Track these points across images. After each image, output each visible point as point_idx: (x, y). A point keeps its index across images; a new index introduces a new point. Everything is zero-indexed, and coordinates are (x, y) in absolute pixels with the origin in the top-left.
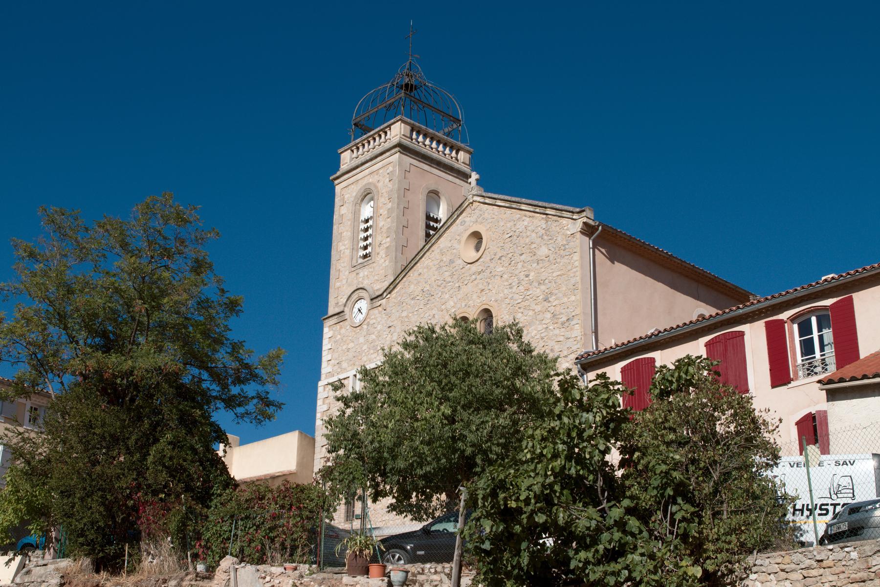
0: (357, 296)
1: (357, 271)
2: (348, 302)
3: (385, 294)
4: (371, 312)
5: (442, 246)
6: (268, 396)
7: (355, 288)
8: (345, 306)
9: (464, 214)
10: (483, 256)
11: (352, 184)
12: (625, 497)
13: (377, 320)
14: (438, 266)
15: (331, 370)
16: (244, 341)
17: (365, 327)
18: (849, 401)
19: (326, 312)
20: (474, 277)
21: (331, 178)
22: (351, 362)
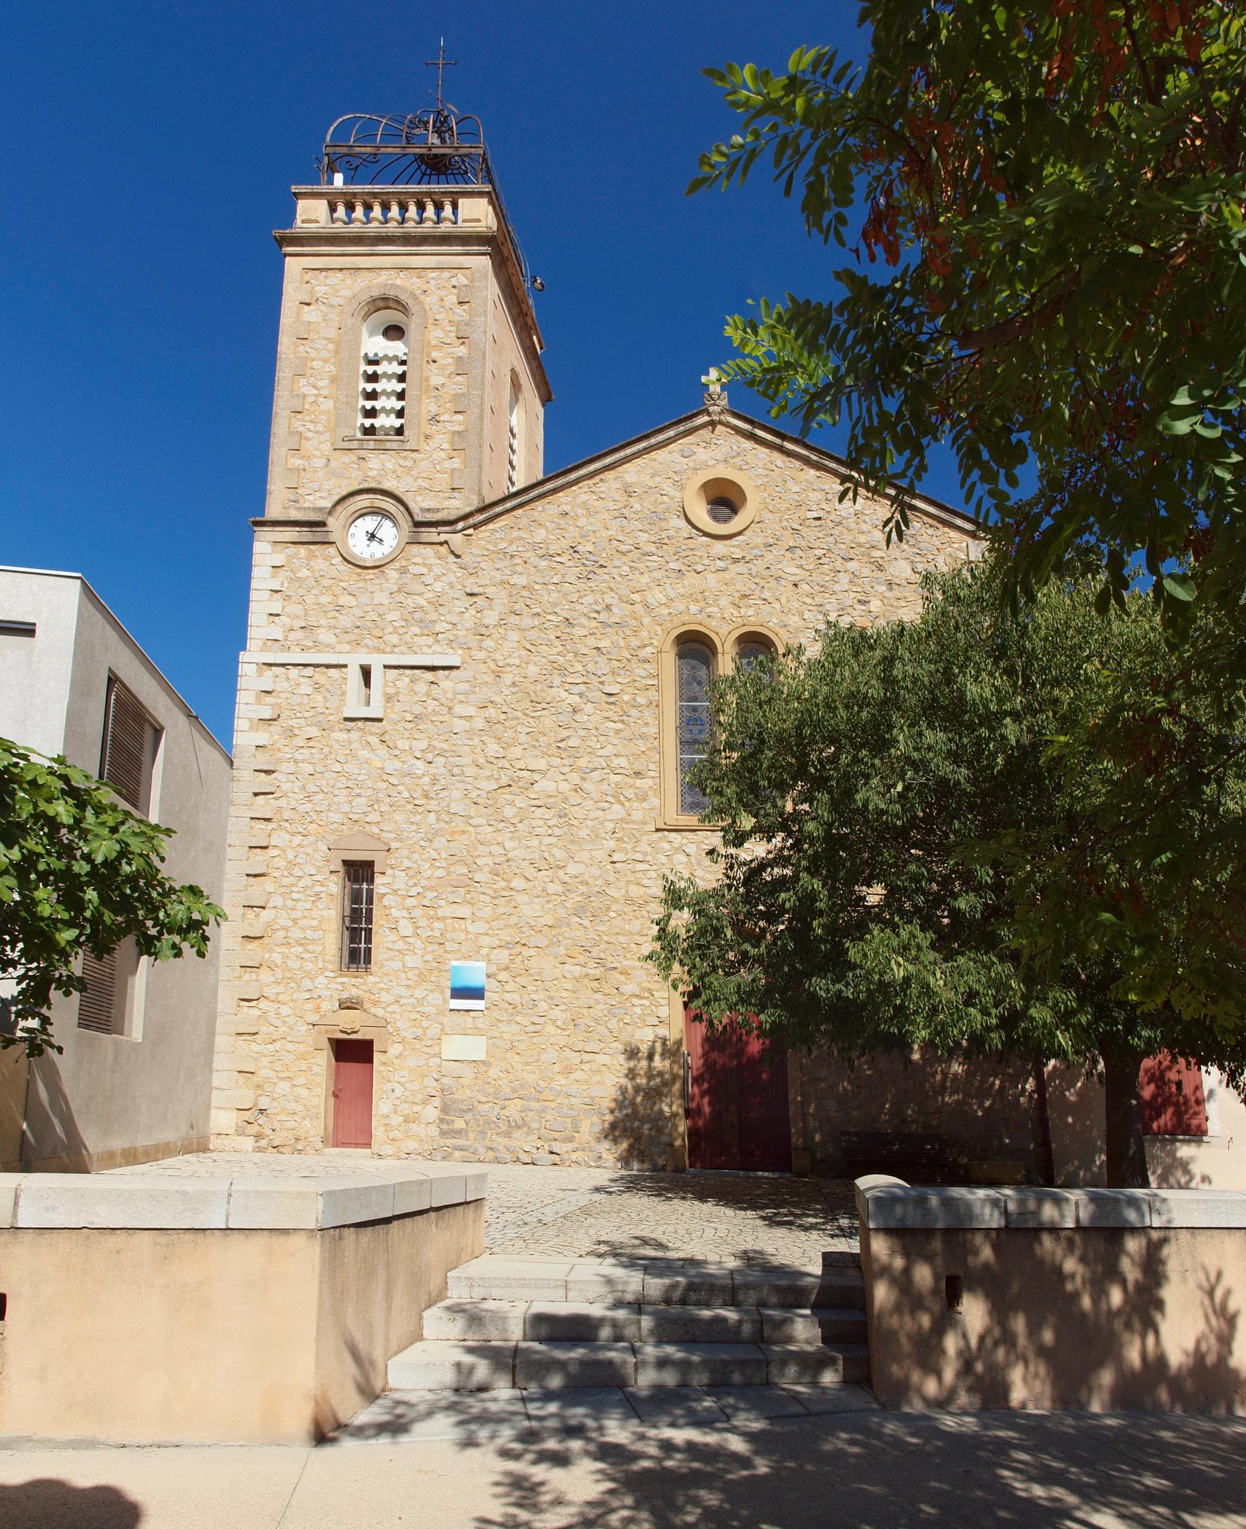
0: (367, 503)
1: (363, 453)
2: (339, 508)
3: (460, 525)
4: (409, 547)
5: (630, 478)
6: (458, 1433)
7: (356, 487)
8: (330, 513)
9: (690, 439)
10: (746, 532)
11: (341, 270)
12: (793, 909)
13: (430, 570)
14: (617, 514)
15: (280, 637)
16: (169, 832)
17: (392, 573)
18: (159, 688)
19: (261, 504)
20: (720, 564)
21: (294, 189)
22: (350, 637)
